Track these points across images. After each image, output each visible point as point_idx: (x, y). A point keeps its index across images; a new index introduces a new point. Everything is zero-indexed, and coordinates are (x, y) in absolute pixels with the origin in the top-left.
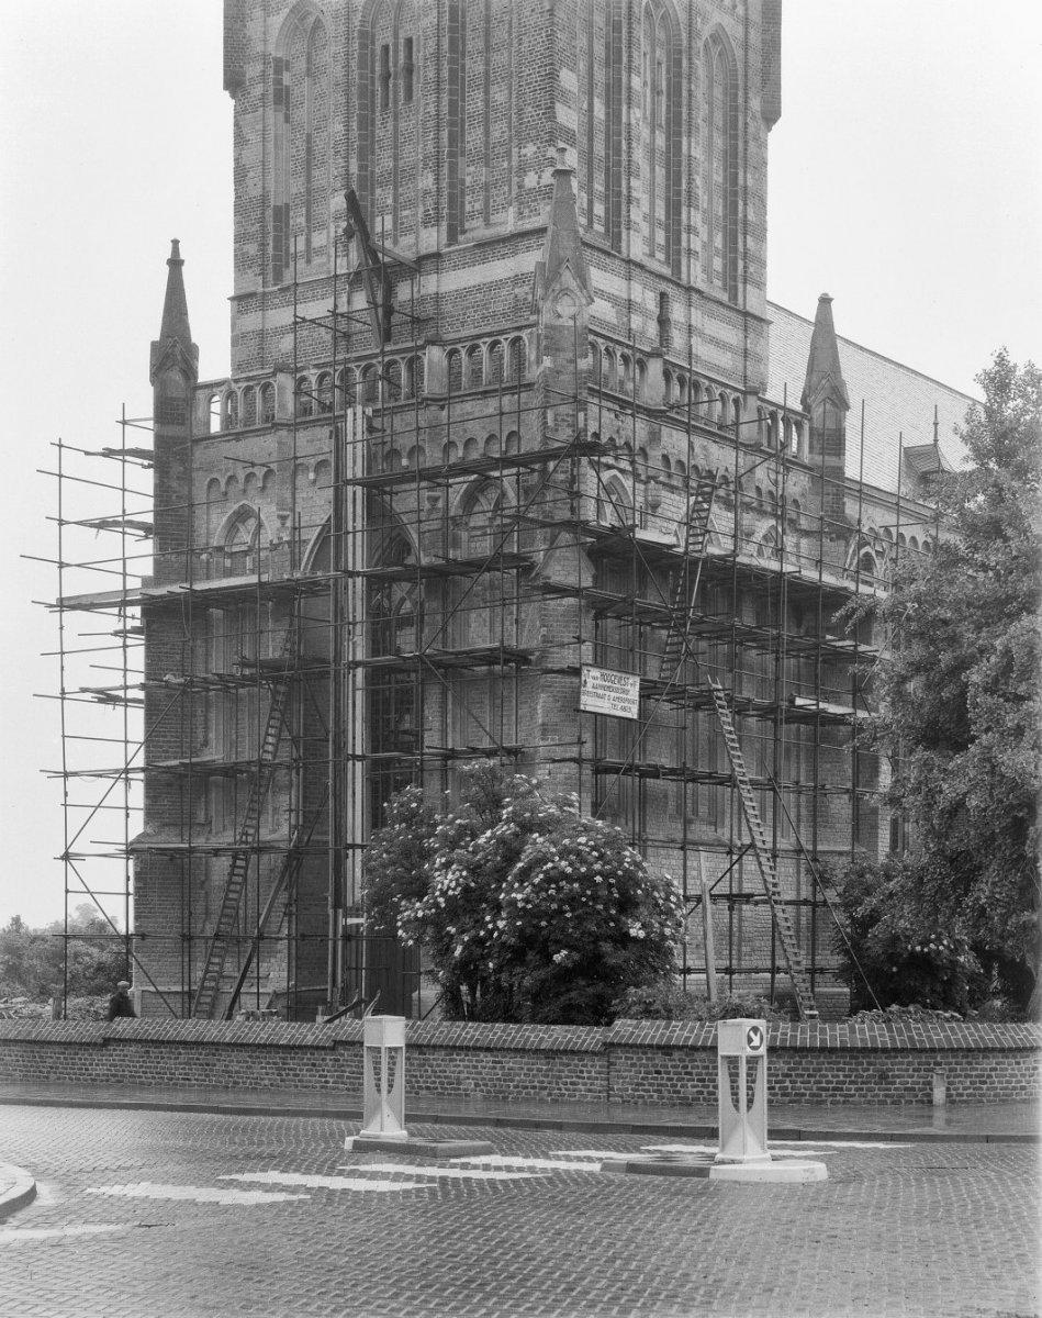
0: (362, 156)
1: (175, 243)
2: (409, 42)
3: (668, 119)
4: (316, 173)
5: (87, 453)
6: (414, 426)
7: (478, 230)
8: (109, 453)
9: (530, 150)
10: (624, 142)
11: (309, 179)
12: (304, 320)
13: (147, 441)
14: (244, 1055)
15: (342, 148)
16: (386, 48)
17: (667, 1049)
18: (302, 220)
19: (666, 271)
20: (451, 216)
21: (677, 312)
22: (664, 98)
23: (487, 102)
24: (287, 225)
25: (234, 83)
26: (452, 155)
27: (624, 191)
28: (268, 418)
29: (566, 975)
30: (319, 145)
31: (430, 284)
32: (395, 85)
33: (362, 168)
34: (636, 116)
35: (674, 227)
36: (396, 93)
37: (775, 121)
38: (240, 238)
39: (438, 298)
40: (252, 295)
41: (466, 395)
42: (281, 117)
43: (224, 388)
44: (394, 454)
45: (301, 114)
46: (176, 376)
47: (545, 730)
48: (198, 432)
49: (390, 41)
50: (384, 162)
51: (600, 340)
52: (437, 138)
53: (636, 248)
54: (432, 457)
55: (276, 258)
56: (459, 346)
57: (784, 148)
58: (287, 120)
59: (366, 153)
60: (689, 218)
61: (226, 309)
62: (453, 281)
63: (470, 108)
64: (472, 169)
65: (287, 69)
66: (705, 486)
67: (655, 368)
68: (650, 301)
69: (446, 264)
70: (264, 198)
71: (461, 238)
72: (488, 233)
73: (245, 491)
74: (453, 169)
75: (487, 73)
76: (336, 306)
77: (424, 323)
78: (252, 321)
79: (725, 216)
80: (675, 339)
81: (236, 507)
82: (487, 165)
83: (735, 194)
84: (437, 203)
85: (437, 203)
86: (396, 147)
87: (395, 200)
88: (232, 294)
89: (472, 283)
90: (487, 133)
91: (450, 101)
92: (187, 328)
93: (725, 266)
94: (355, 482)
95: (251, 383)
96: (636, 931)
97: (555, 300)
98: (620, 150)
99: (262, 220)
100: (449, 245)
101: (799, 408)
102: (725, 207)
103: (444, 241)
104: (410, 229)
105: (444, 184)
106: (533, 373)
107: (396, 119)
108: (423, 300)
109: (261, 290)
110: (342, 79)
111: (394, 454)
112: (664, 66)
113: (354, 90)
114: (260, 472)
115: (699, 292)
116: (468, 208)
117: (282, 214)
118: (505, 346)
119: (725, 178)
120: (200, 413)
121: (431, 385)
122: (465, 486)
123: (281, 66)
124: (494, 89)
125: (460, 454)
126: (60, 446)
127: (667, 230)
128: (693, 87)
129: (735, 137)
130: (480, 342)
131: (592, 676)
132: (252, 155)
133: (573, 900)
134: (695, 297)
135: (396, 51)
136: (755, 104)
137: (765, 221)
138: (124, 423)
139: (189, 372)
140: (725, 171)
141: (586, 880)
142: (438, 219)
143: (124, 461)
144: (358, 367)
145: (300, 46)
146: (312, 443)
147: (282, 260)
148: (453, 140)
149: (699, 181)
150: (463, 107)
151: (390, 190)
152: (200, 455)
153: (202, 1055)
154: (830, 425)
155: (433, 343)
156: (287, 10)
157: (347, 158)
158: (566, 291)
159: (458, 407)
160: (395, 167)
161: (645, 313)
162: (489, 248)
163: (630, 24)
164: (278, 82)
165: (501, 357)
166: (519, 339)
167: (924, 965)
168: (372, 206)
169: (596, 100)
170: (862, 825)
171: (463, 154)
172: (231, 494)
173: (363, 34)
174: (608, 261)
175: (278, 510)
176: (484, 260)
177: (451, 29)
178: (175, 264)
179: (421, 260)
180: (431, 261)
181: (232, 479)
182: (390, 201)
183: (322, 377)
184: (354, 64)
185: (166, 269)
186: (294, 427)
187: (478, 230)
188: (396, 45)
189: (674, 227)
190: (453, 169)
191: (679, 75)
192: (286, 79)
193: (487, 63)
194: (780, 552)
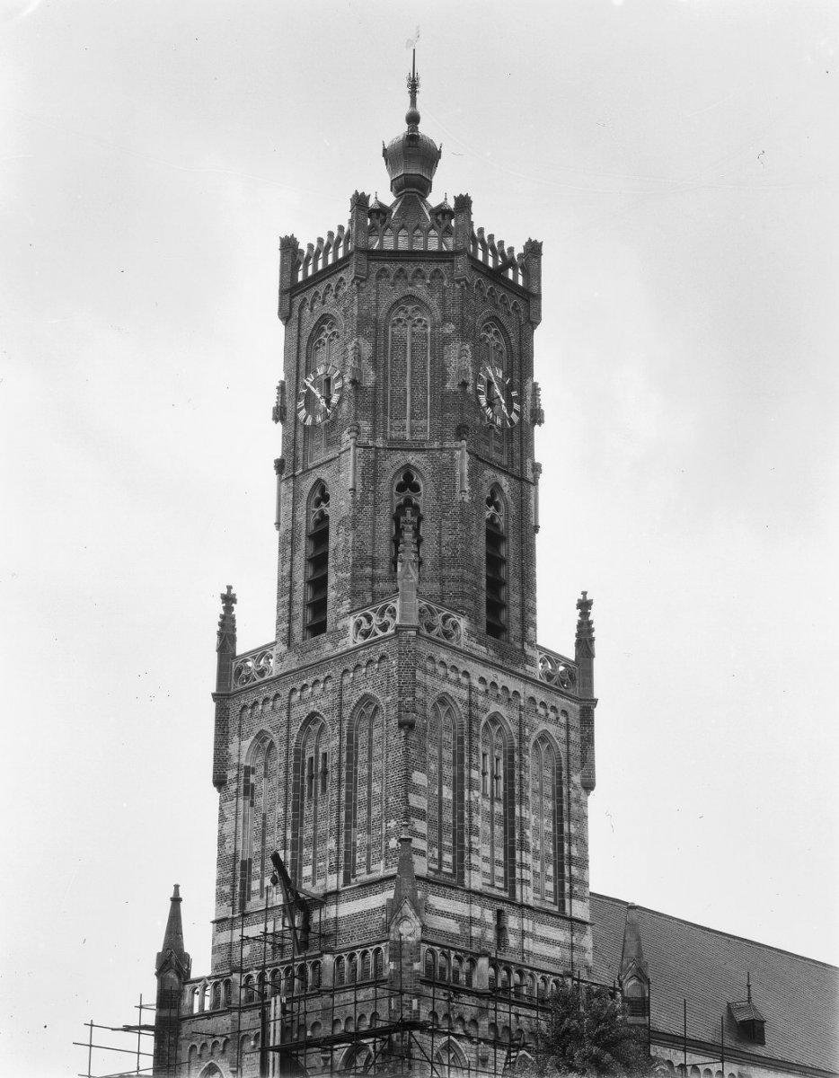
0: (294, 829)
1: (177, 887)
2: (325, 755)
3: (505, 794)
4: (268, 838)
5: (113, 1029)
6: (353, 1001)
7: (362, 875)
8: (128, 1029)
9: (393, 823)
10: (466, 813)
11: (264, 843)
12: (248, 938)
13: (150, 1018)
15: (282, 823)
16: (311, 759)
18: (258, 869)
19: (504, 894)
20: (346, 867)
21: (512, 922)
22: (501, 782)
23: (369, 793)
24: (250, 872)
25: (220, 782)
26: (347, 827)
27: (467, 845)
28: (228, 1002)
30: (271, 821)
31: (331, 911)
33: (294, 835)
36: (316, 789)
37: (592, 789)
38: (220, 882)
40: (225, 919)
41: (347, 987)
42: (248, 802)
43: (202, 983)
44: (303, 1028)
45: (260, 801)
46: (172, 975)
48: (185, 1013)
49: (313, 755)
50: (308, 832)
51: (436, 948)
52: (338, 817)
53: (476, 881)
54: (325, 1031)
56: (343, 954)
57: (597, 806)
58: (252, 804)
59: (297, 825)
60: (521, 858)
61: (210, 928)
62: (346, 909)
63: (360, 797)
64: (360, 835)
65: (253, 773)
68: (489, 917)
69: (342, 898)
70: (235, 855)
71: (353, 880)
73: (212, 1054)
74: (348, 836)
75: (370, 775)
76: (266, 929)
77: (327, 937)
78: (225, 937)
79: (555, 853)
80: (511, 941)
81: (206, 1064)
82: (369, 833)
83: (562, 839)
84: (338, 858)
85: (338, 858)
86: (315, 821)
87: (314, 856)
88: (214, 919)
89: (357, 911)
90: (369, 813)
91: (347, 792)
92: (182, 944)
93: (555, 887)
94: (275, 1049)
95: (218, 980)
97: (398, 924)
98: (463, 818)
99: (234, 870)
100: (345, 886)
102: (554, 849)
103: (341, 882)
104: (324, 875)
105: (342, 845)
107: (316, 804)
108: (327, 922)
109: (231, 915)
110: (283, 780)
111: (303, 1028)
112: (501, 762)
113: (290, 786)
114: (221, 1041)
116: (358, 861)
117: (246, 866)
118: (358, 956)
119: (554, 829)
120: (187, 1001)
121: (327, 982)
122: (346, 1049)
123: (249, 771)
124: (374, 784)
125: (343, 1028)
126: (92, 1025)
128: (523, 772)
129: (561, 801)
130: (355, 952)
134: (526, 911)
135: (317, 762)
136: (576, 779)
137: (587, 855)
138: (141, 1007)
140: (554, 823)
142: (338, 868)
143: (140, 1033)
144: (282, 968)
145: (260, 759)
146: (249, 1020)
147: (246, 895)
148: (348, 817)
149: (529, 833)
150: (356, 796)
151: (311, 850)
152: (186, 1029)
154: (637, 994)
156: (253, 737)
158: (405, 918)
159: (342, 995)
160: (315, 835)
163: (470, 738)
164: (247, 781)
165: (356, 965)
166: (379, 949)
168: (301, 860)
169: (444, 787)
171: (355, 827)
172: (204, 1056)
173: (297, 752)
174: (453, 892)
175: (231, 1067)
176: (365, 896)
177: (348, 748)
178: (176, 901)
179: (327, 895)
180: (333, 896)
181: (204, 1045)
182: (311, 857)
183: (287, 971)
184: (291, 770)
185: (169, 903)
186: (241, 1009)
187: (362, 875)
188: (317, 757)
190: (348, 836)
191: (513, 766)
192: (252, 779)
193: (370, 768)
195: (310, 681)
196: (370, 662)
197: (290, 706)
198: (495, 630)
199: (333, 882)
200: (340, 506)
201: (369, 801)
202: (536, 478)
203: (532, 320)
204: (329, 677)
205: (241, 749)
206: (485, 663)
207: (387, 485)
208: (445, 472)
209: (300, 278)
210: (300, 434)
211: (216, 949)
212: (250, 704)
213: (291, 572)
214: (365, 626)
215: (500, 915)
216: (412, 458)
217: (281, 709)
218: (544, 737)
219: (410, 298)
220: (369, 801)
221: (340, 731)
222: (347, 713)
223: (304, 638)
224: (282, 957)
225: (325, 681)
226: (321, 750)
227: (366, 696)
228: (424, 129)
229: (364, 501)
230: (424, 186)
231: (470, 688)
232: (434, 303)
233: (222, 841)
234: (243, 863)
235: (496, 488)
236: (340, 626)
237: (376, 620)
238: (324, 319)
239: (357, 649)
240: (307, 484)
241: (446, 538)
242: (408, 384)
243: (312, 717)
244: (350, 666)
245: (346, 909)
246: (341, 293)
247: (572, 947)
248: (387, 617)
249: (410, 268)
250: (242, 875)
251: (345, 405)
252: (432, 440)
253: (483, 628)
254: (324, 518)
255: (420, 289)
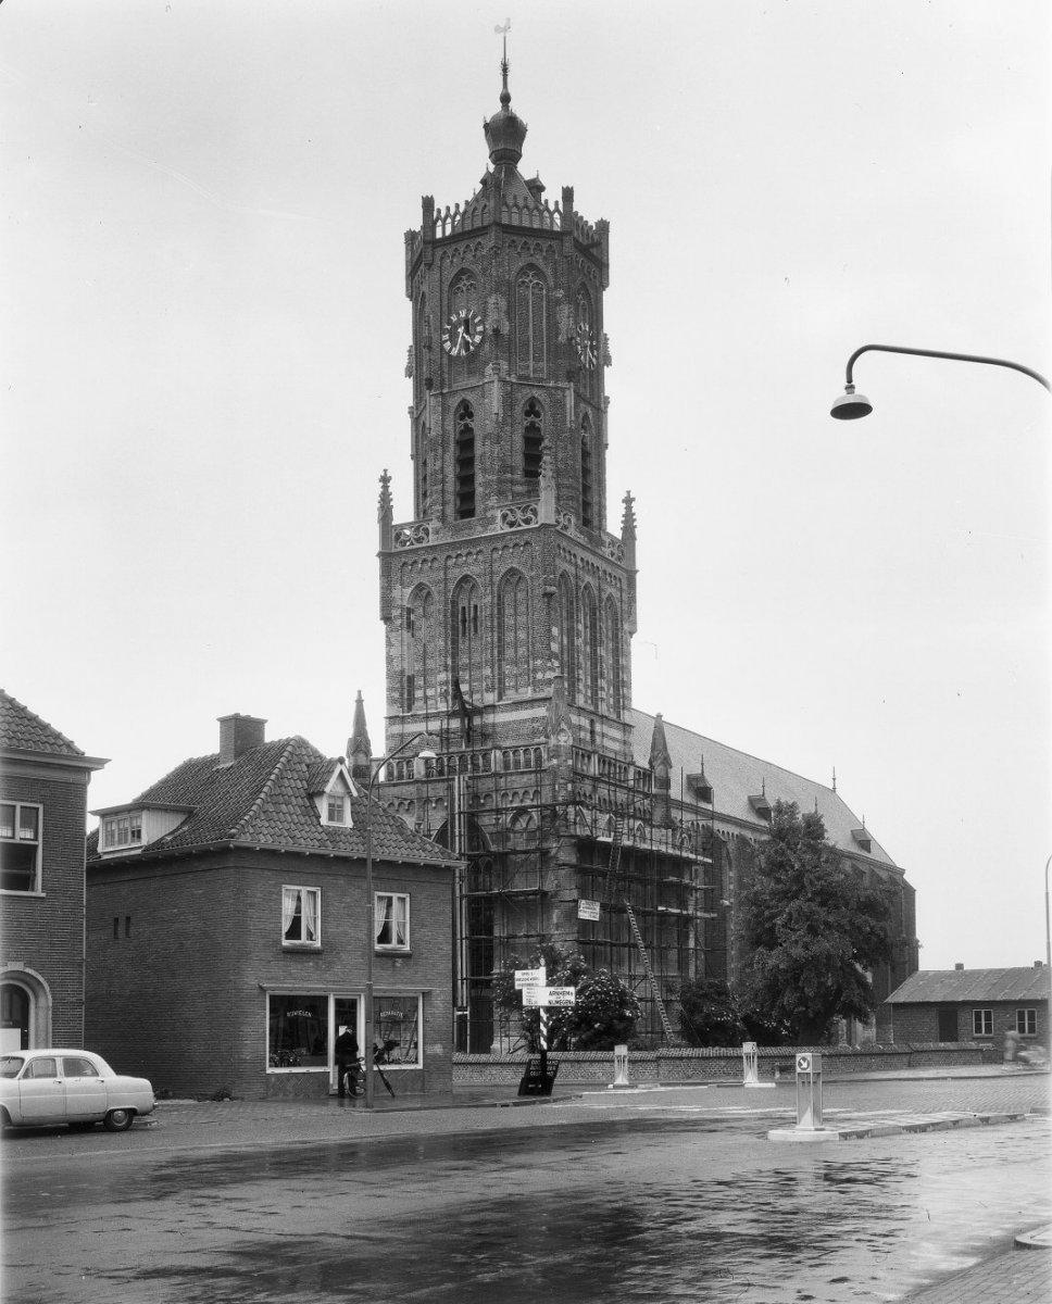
1: (359, 692)
2: (476, 607)
4: (428, 661)
9: (539, 662)
11: (425, 664)
14: (499, 1067)
17: (681, 1058)
18: (422, 683)
19: (592, 708)
21: (598, 728)
25: (387, 619)
26: (499, 660)
29: (599, 1033)
31: (490, 718)
32: (469, 626)
33: (453, 662)
34: (579, 642)
35: (595, 688)
38: (390, 690)
39: (494, 725)
47: (558, 926)
49: (466, 605)
50: (464, 660)
55: (409, 699)
59: (455, 656)
62: (501, 718)
63: (508, 640)
66: (620, 812)
67: (595, 758)
70: (402, 672)
72: (518, 698)
74: (500, 667)
78: (397, 729)
90: (516, 652)
96: (628, 1013)
101: (647, 766)
103: (496, 698)
106: (546, 765)
114: (406, 803)
115: (606, 717)
117: (411, 680)
123: (410, 611)
127: (592, 689)
131: (583, 903)
132: (395, 652)
133: (602, 1002)
135: (469, 611)
139: (367, 753)
141: (607, 993)
146: (440, 790)
147: (411, 701)
153: (478, 1068)
154: (663, 774)
155: (496, 748)
157: (446, 657)
161: (585, 730)
162: (518, 705)
167: (721, 1027)
170: (682, 965)
178: (360, 702)
180: (492, 708)
182: (467, 678)
189: (595, 688)
190: (500, 667)
192: (412, 617)
194: (644, 839)
195: (464, 552)
196: (516, 545)
197: (446, 568)
198: (586, 522)
199: (490, 698)
200: (483, 424)
201: (516, 644)
202: (606, 407)
203: (602, 283)
204: (480, 551)
205: (403, 595)
206: (584, 547)
207: (519, 410)
208: (559, 405)
209: (439, 235)
210: (445, 361)
211: (389, 737)
212: (410, 562)
213: (443, 467)
214: (510, 518)
215: (592, 722)
216: (536, 393)
217: (438, 569)
218: (609, 598)
219: (531, 266)
220: (516, 644)
221: (492, 593)
222: (497, 579)
223: (456, 519)
224: (448, 749)
225: (477, 554)
226: (472, 603)
227: (512, 569)
228: (516, 107)
229: (504, 422)
230: (515, 156)
231: (576, 566)
232: (549, 272)
233: (390, 660)
234: (409, 677)
235: (586, 416)
236: (489, 515)
237: (519, 514)
238: (463, 271)
239: (504, 535)
240: (454, 402)
241: (560, 455)
242: (531, 333)
243: (466, 578)
244: (499, 545)
245: (501, 718)
246: (478, 253)
247: (625, 743)
248: (529, 514)
249: (532, 242)
250: (409, 686)
251: (487, 346)
252: (549, 379)
253: (581, 522)
254: (468, 430)
255: (539, 260)
